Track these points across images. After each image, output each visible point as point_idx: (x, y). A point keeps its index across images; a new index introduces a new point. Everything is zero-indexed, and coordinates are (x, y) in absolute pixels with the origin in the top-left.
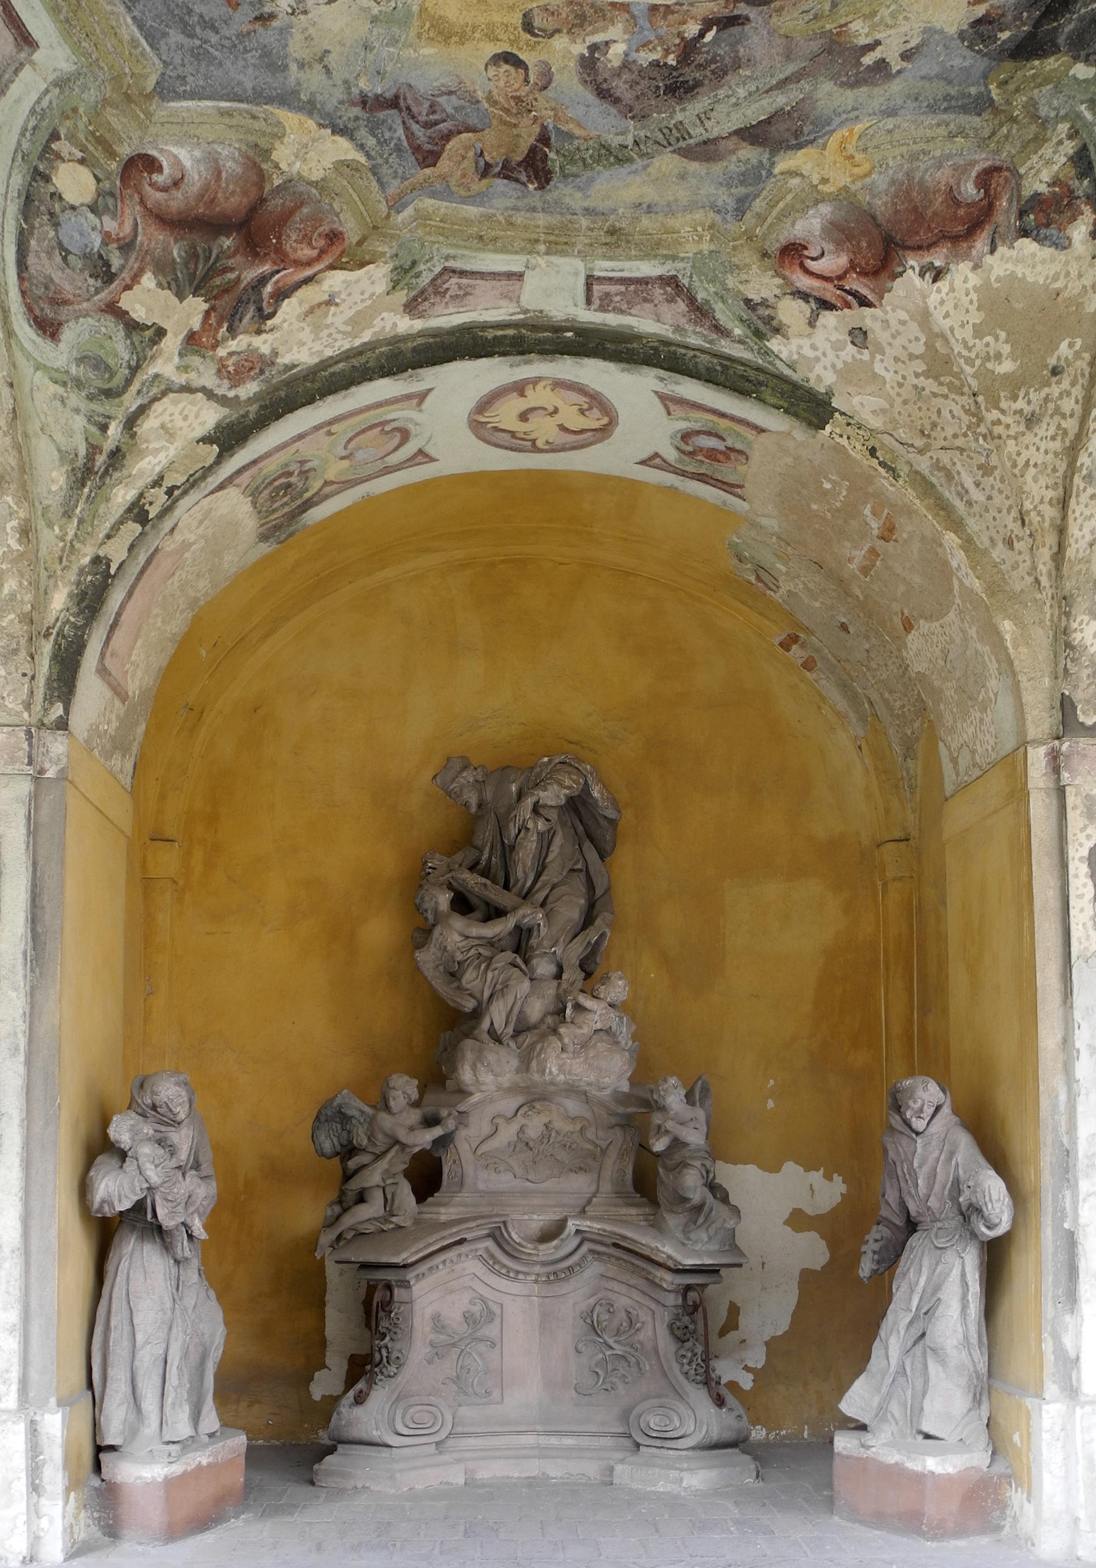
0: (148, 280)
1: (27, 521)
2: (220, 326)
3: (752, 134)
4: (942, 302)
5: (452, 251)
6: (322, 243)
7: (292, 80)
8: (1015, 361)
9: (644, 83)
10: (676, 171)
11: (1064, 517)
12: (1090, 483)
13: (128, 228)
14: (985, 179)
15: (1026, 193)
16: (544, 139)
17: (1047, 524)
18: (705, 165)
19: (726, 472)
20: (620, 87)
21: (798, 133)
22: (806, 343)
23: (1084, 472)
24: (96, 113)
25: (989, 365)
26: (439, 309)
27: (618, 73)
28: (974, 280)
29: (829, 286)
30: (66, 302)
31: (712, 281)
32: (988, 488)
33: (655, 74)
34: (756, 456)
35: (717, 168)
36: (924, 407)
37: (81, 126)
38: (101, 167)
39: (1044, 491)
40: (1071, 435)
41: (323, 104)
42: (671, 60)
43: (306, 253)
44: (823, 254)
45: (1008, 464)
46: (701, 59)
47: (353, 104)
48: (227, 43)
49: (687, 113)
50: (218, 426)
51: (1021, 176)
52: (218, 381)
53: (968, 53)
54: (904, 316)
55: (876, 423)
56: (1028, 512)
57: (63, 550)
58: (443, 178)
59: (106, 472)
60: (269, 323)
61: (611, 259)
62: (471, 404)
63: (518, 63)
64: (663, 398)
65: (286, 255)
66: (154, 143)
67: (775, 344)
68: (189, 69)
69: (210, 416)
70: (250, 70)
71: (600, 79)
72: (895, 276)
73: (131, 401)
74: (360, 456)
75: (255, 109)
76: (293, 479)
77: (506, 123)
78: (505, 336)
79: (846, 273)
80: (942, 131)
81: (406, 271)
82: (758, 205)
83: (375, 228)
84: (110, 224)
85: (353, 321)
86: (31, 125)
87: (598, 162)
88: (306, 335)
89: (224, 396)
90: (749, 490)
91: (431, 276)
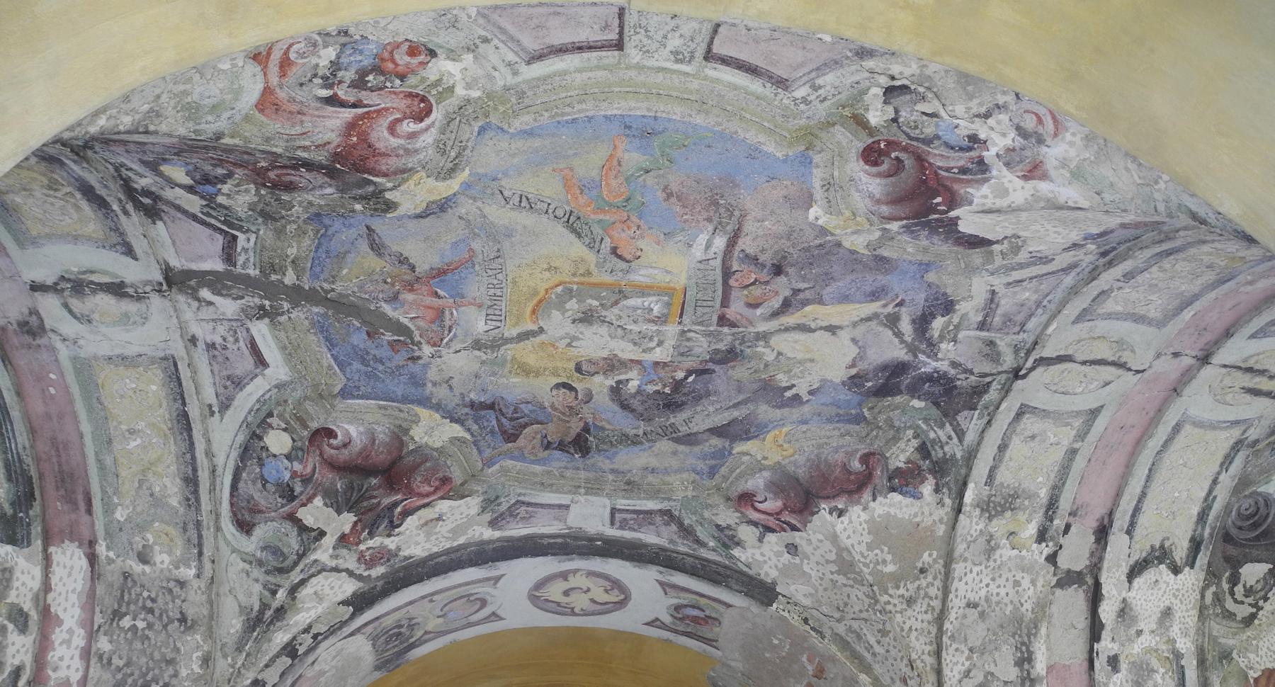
0: (318, 501)
1: (209, 653)
2: (363, 531)
3: (717, 431)
4: (845, 529)
5: (523, 491)
6: (437, 483)
7: (428, 392)
8: (895, 564)
9: (650, 402)
10: (670, 450)
11: (940, 663)
12: (954, 641)
13: (309, 470)
14: (865, 459)
15: (892, 467)
16: (586, 429)
17: (928, 668)
18: (689, 447)
19: (705, 631)
20: (635, 403)
21: (747, 432)
22: (757, 552)
23: (949, 634)
24: (299, 403)
25: (879, 567)
26: (512, 525)
27: (634, 396)
28: (864, 516)
30: (260, 512)
31: (694, 513)
32: (886, 645)
33: (657, 397)
34: (726, 622)
35: (697, 449)
36: (839, 593)
37: (288, 410)
38: (298, 434)
39: (923, 646)
40: (937, 611)
41: (446, 405)
42: (667, 390)
43: (427, 489)
44: (766, 500)
45: (898, 629)
46: (686, 390)
47: (466, 406)
48: (388, 370)
49: (678, 419)
50: (354, 594)
51: (887, 458)
52: (357, 565)
53: (848, 392)
54: (821, 537)
55: (806, 602)
56: (915, 660)
57: (232, 674)
58: (520, 449)
59: (272, 622)
60: (397, 530)
61: (627, 498)
62: (531, 585)
63: (571, 388)
64: (662, 584)
65: (413, 490)
66: (334, 423)
67: (736, 552)
68: (363, 383)
69: (349, 587)
70: (402, 385)
71: (623, 398)
72: (813, 514)
73: (295, 576)
74: (451, 615)
75: (402, 406)
76: (402, 630)
77: (562, 420)
78: (556, 543)
79: (781, 511)
80: (836, 433)
81: (492, 502)
82: (723, 470)
83: (473, 476)
84: (297, 466)
85: (453, 531)
86: (255, 408)
87: (621, 443)
88: (421, 538)
89: (361, 575)
90: (721, 643)
91: (509, 505)
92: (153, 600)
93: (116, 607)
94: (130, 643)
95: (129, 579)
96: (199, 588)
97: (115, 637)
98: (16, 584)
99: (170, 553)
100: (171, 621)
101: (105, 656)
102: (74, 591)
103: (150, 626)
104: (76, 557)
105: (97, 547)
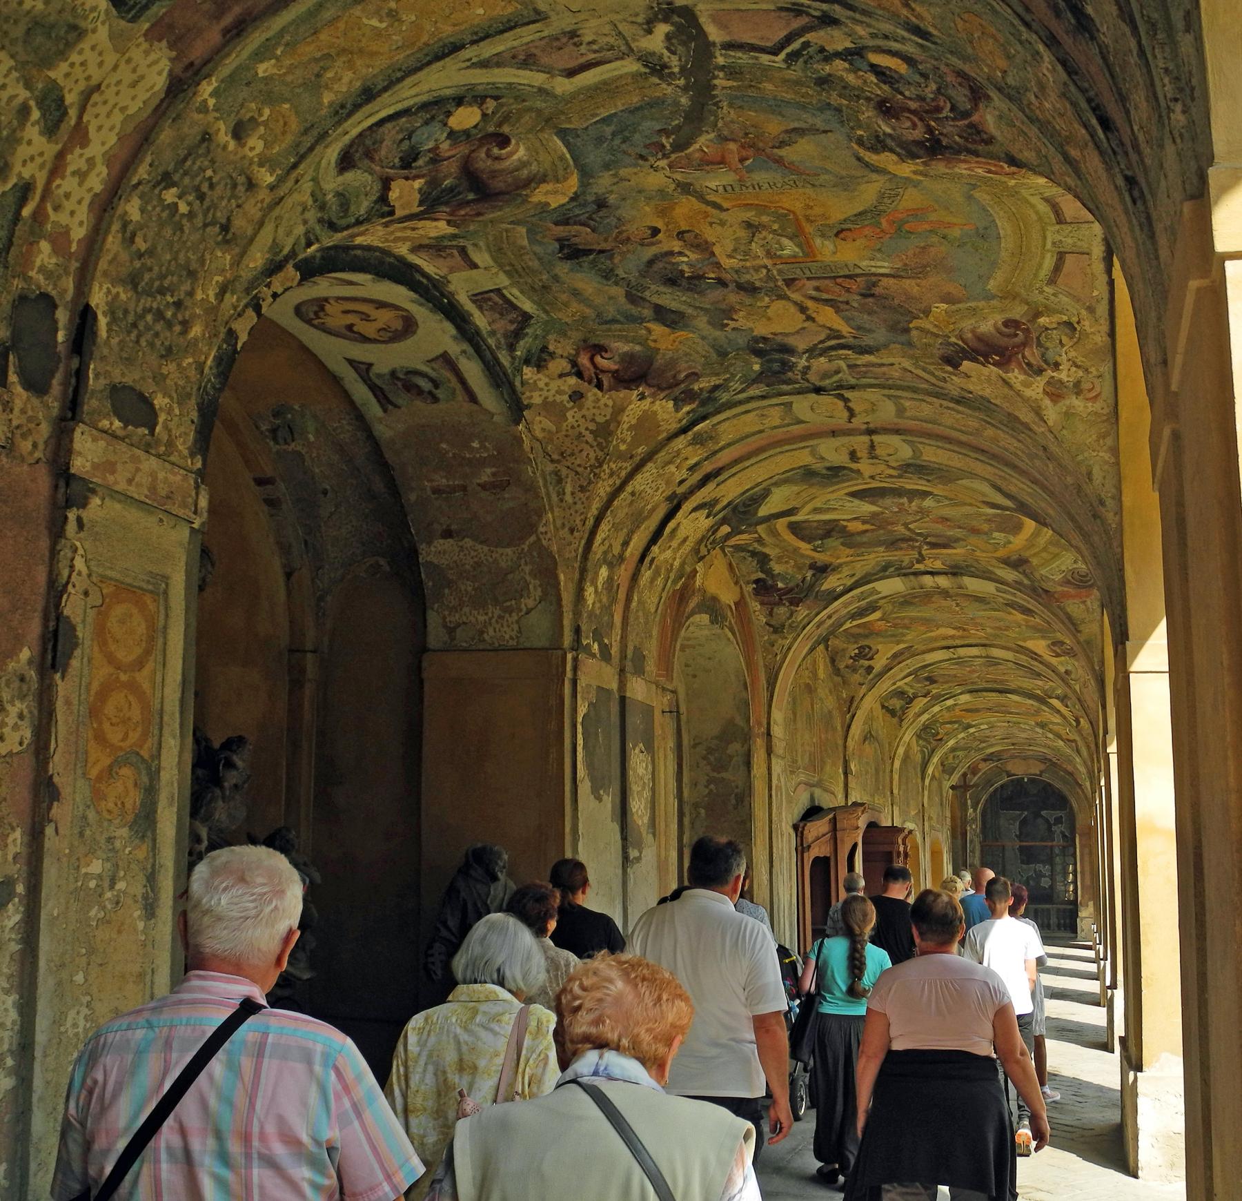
29: (592, 370)
92: (212, 186)
93: (171, 168)
94: (162, 225)
95: (205, 145)
96: (262, 201)
97: (150, 208)
98: (75, 57)
99: (267, 145)
100: (213, 223)
101: (131, 228)
102: (123, 109)
103: (191, 215)
104: (156, 68)
105: (204, 83)
